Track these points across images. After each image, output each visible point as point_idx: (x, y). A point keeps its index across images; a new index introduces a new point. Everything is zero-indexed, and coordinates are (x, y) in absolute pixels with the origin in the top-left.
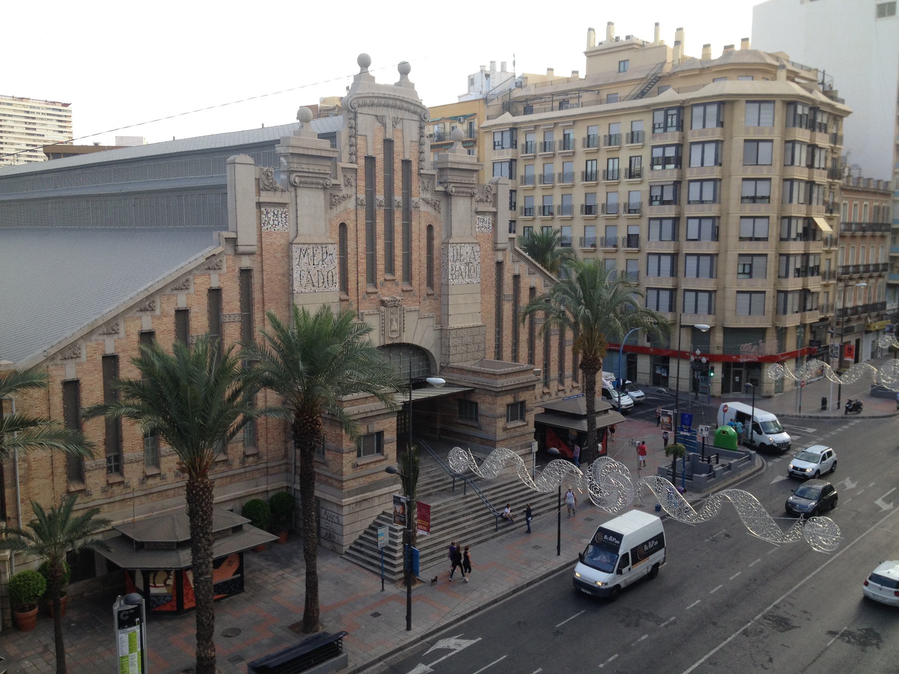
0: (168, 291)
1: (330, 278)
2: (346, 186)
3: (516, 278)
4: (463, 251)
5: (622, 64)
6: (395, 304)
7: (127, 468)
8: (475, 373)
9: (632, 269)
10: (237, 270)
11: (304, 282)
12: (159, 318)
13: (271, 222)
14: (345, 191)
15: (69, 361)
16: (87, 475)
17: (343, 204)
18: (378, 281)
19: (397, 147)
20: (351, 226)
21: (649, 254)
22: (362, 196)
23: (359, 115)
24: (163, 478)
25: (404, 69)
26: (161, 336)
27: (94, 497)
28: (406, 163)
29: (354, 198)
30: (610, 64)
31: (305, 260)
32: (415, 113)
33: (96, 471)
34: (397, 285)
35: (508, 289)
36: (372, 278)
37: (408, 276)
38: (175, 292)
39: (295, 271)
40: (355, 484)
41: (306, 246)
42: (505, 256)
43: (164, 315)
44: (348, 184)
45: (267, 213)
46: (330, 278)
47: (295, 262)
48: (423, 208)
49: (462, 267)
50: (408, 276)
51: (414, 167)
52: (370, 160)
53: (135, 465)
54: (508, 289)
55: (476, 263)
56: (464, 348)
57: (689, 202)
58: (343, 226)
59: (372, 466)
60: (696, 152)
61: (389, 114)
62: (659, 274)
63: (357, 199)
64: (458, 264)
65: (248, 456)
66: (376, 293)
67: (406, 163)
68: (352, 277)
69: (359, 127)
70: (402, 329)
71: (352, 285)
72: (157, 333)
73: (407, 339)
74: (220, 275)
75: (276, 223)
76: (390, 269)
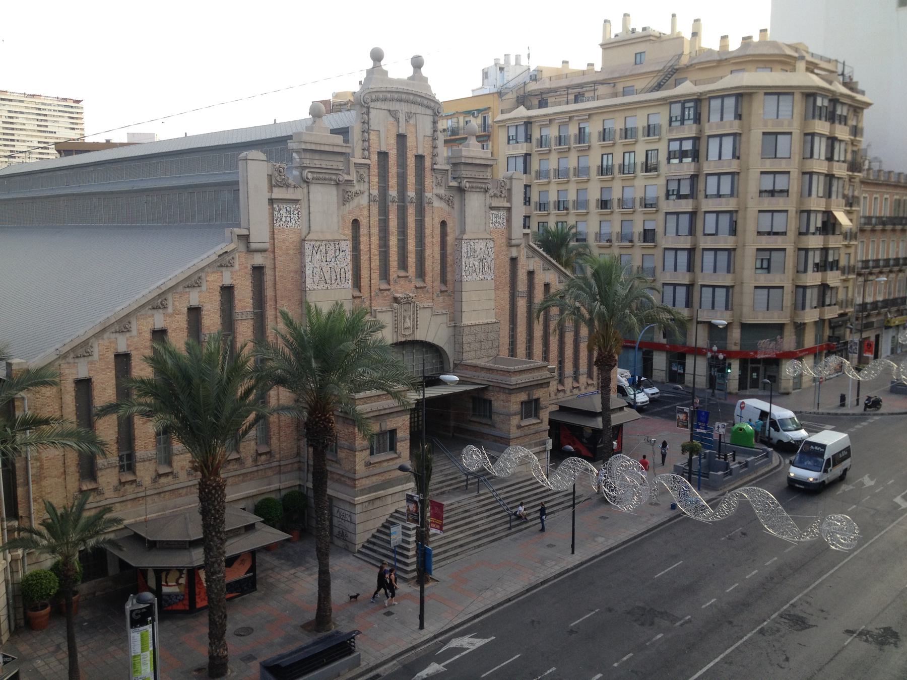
0: (180, 288)
1: (343, 275)
2: (359, 181)
3: (531, 274)
4: (477, 247)
5: (638, 56)
6: (408, 301)
7: (139, 467)
8: (489, 370)
9: (648, 264)
10: (249, 267)
11: (317, 279)
12: (171, 316)
13: (284, 219)
14: (357, 187)
15: (82, 360)
16: (99, 474)
17: (356, 200)
18: (391, 278)
19: (411, 142)
20: (364, 223)
21: (666, 249)
22: (375, 192)
23: (371, 110)
24: (175, 476)
25: (417, 63)
26: (173, 334)
27: (106, 496)
28: (420, 158)
29: (366, 194)
30: (626, 56)
31: (318, 257)
32: (428, 107)
33: (108, 470)
34: (410, 281)
35: (522, 286)
36: (385, 274)
37: (421, 273)
38: (187, 290)
39: (307, 268)
40: (367, 482)
41: (319, 243)
42: (519, 252)
43: (176, 312)
44: (361, 179)
45: (280, 209)
46: (343, 275)
47: (308, 259)
48: (437, 203)
49: (476, 263)
50: (421, 273)
51: (428, 162)
52: (383, 155)
53: (147, 463)
54: (522, 286)
55: (489, 259)
56: (478, 345)
57: (706, 196)
58: (356, 222)
59: (385, 464)
60: (714, 145)
61: (403, 109)
62: (675, 270)
63: (370, 194)
64: (471, 260)
65: (260, 455)
66: (389, 290)
67: (420, 158)
68: (364, 273)
69: (372, 122)
70: (415, 327)
71: (364, 282)
72: (169, 331)
73: (420, 336)
74: (232, 272)
75: (289, 219)
76: (403, 265)
